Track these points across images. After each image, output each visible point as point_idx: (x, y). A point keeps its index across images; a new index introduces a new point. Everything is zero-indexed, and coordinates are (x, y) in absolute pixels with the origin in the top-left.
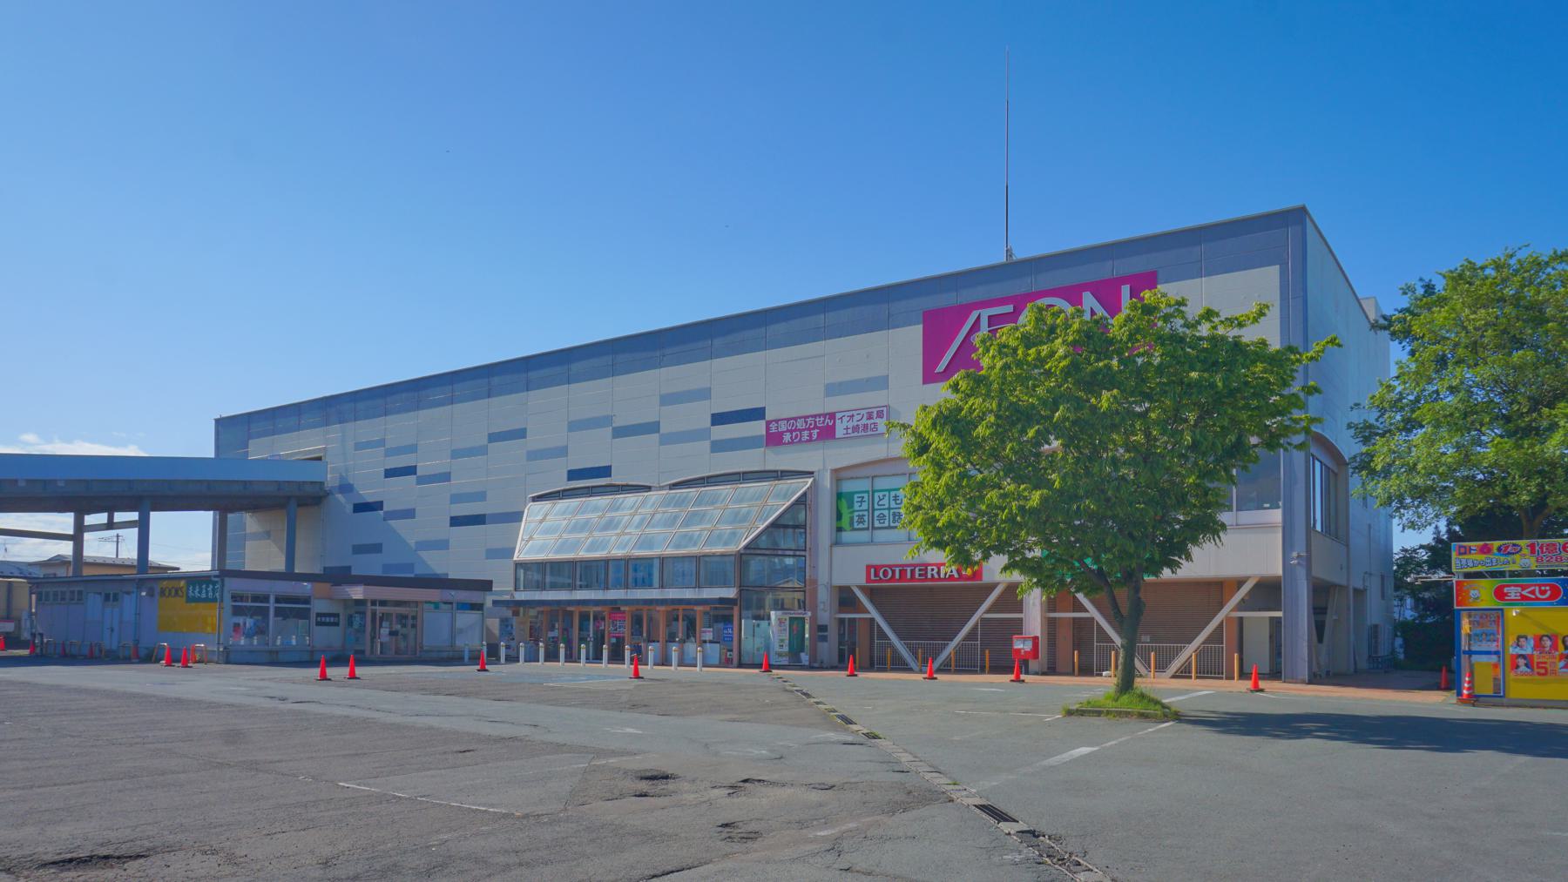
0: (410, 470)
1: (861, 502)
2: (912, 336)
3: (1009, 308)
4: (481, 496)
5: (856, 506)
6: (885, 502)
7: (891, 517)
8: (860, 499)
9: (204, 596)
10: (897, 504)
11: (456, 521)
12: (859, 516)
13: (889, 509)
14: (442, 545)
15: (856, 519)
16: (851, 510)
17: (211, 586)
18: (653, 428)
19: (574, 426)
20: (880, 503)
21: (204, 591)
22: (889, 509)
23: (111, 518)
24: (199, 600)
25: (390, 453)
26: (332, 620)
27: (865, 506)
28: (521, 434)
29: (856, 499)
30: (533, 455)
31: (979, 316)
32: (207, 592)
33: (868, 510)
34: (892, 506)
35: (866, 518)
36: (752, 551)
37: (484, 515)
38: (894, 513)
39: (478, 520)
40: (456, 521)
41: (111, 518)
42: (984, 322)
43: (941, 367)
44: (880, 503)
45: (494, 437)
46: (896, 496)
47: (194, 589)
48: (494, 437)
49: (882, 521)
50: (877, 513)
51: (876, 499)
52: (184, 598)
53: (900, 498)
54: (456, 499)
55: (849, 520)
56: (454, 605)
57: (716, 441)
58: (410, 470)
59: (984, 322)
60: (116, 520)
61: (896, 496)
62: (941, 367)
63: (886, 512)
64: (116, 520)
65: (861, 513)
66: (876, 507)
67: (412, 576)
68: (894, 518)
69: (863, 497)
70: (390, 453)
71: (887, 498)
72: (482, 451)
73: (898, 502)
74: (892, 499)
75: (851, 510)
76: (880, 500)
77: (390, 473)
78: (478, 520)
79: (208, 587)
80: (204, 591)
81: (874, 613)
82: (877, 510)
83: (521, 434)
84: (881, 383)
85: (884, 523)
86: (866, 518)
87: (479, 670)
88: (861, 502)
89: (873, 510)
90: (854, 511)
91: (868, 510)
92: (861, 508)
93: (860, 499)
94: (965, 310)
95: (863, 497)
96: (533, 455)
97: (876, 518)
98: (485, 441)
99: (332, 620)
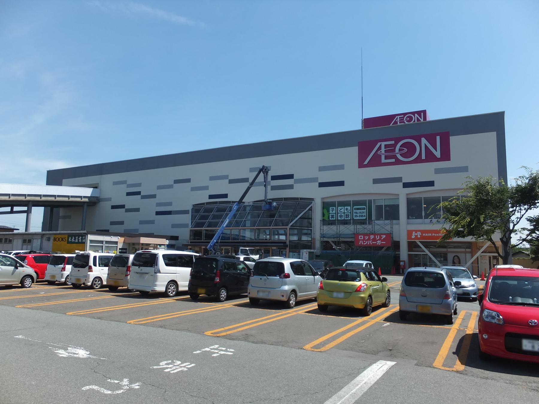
0: (138, 193)
1: (333, 210)
2: (354, 151)
3: (393, 142)
4: (170, 204)
5: (331, 212)
6: (343, 210)
7: (345, 216)
8: (332, 209)
9: (77, 241)
10: (347, 211)
11: (158, 213)
12: (332, 215)
13: (344, 213)
14: (152, 222)
15: (330, 216)
16: (328, 213)
17: (80, 238)
18: (232, 181)
19: (212, 178)
20: (340, 211)
21: (77, 239)
22: (344, 213)
23: (12, 209)
24: (71, 243)
25: (129, 186)
26: (124, 251)
27: (334, 212)
28: (188, 181)
29: (330, 209)
30: (193, 189)
31: (381, 144)
32: (78, 240)
33: (336, 213)
34: (345, 212)
35: (335, 216)
36: (293, 227)
37: (171, 211)
38: (346, 215)
39: (169, 213)
40: (158, 213)
41: (12, 209)
42: (383, 147)
43: (366, 163)
44: (340, 211)
45: (176, 182)
46: (347, 208)
47: (72, 238)
48: (176, 182)
49: (341, 217)
50: (339, 214)
51: (339, 209)
52: (66, 241)
53: (349, 209)
54: (158, 205)
55: (327, 217)
56: (166, 246)
57: (125, 184)
58: (138, 193)
59: (383, 147)
60: (10, 208)
61: (347, 208)
62: (366, 163)
63: (343, 214)
64: (10, 208)
65: (333, 214)
66: (339, 212)
67: (138, 233)
68: (346, 217)
69: (333, 209)
70: (129, 186)
71: (343, 209)
72: (170, 187)
73: (348, 211)
74: (345, 209)
75: (328, 213)
76: (340, 210)
77: (128, 194)
78: (169, 213)
79: (79, 237)
80: (77, 239)
81: (427, 252)
82: (344, 215)
83: (188, 181)
84: (341, 167)
85: (342, 218)
86: (335, 216)
87: (481, 280)
88: (333, 210)
89: (338, 213)
90: (330, 213)
91: (336, 213)
92: (332, 213)
93: (332, 209)
94: (375, 143)
95: (333, 209)
96: (193, 189)
97: (339, 216)
98: (172, 183)
99: (124, 251)
